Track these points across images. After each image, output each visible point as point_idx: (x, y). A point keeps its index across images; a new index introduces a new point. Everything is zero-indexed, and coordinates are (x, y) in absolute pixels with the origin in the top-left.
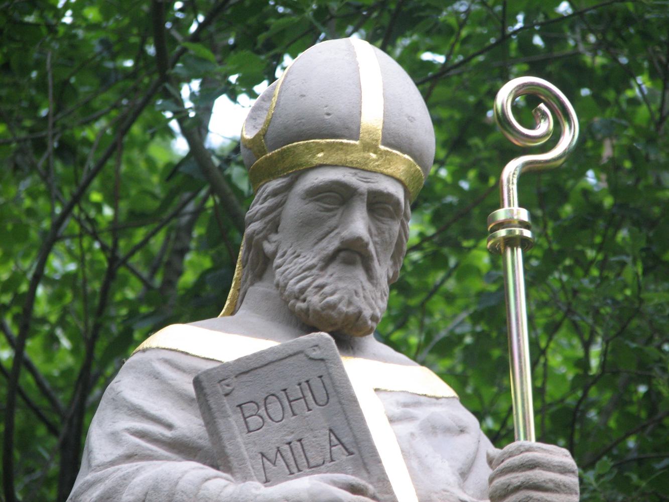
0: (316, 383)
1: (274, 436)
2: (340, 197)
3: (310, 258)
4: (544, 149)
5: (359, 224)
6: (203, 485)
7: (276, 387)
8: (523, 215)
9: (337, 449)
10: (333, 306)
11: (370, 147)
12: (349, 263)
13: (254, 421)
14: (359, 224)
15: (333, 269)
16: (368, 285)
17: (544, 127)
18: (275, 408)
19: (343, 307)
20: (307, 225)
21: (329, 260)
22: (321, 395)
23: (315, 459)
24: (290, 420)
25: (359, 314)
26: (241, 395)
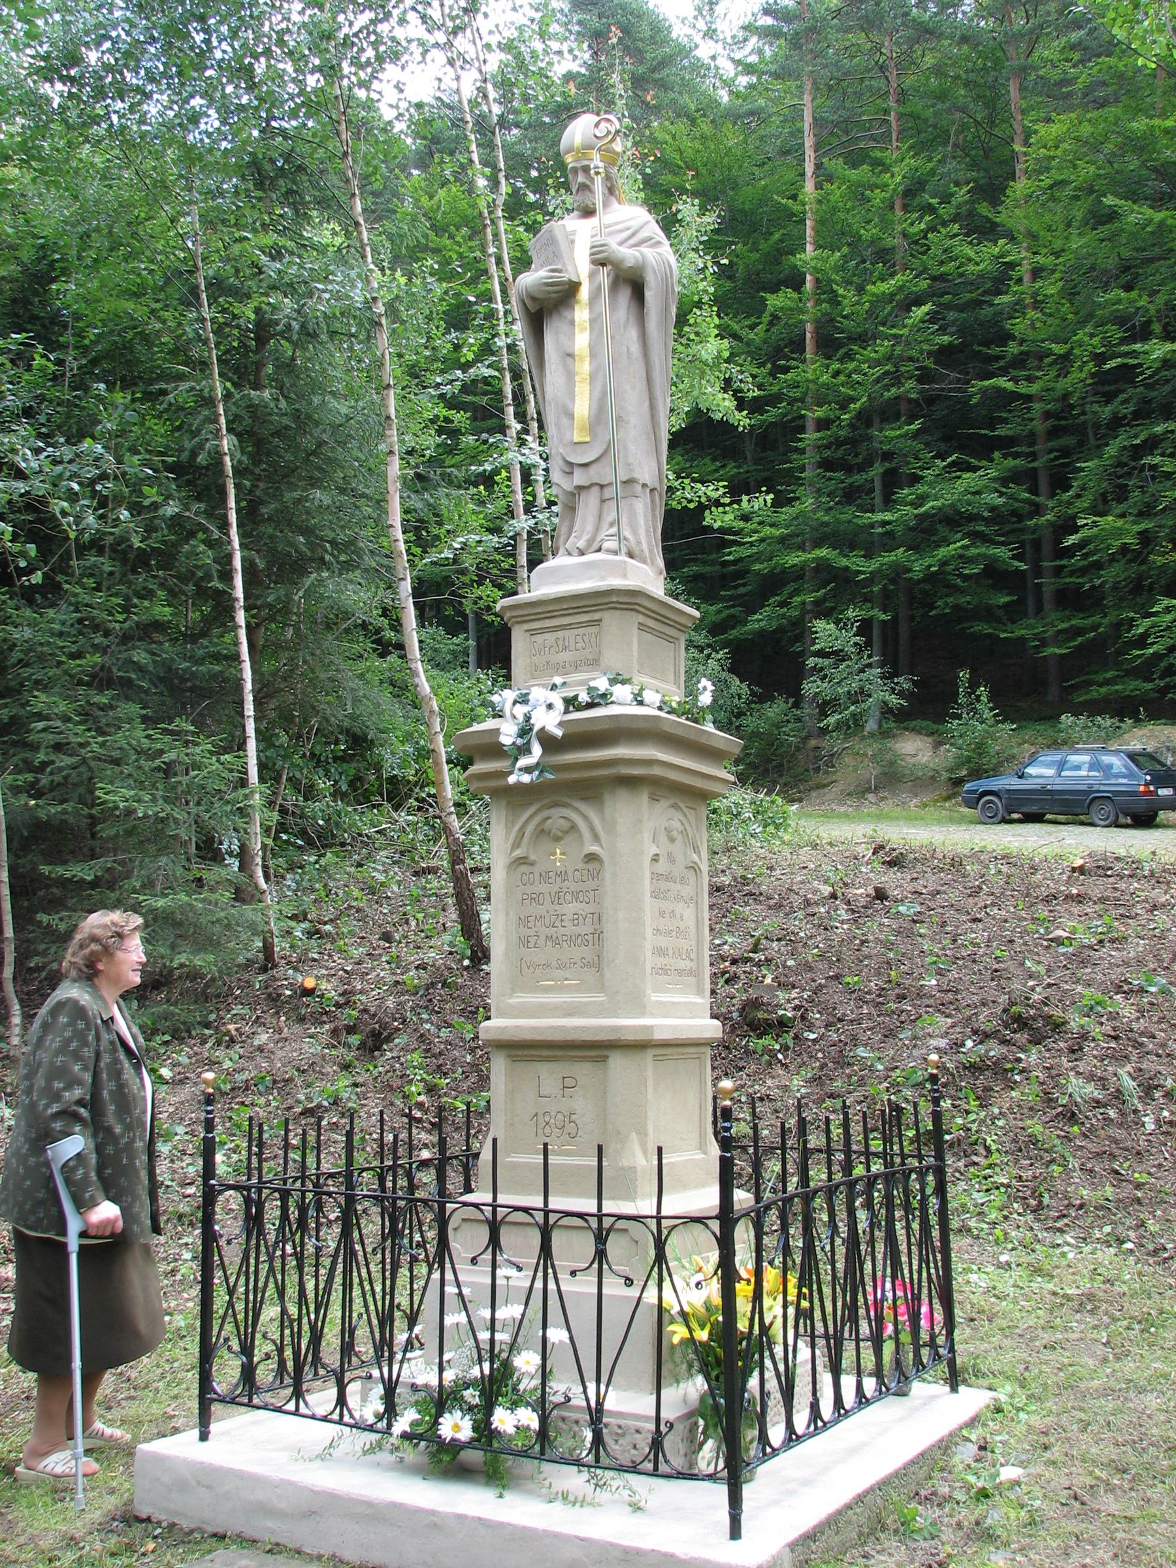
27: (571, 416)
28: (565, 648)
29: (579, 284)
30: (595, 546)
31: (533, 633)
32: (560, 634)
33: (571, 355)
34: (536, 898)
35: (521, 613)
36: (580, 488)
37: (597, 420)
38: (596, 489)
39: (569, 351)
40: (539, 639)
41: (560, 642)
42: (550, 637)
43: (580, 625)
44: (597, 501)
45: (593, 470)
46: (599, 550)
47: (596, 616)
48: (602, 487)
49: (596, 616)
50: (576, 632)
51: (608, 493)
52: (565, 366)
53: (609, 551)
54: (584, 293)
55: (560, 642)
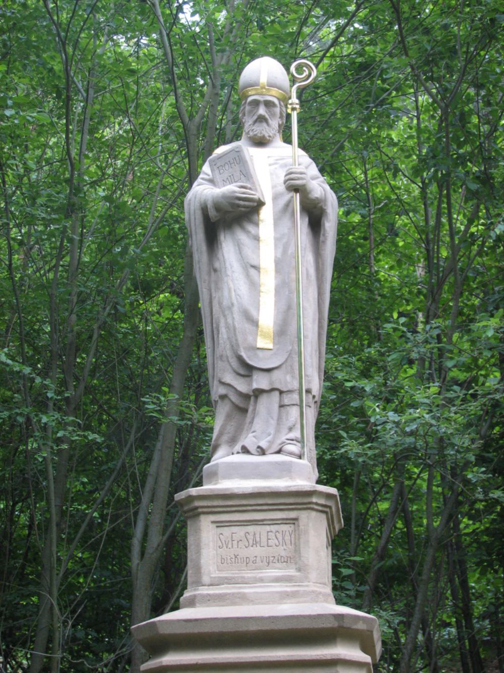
0: (237, 158)
1: (226, 175)
2: (256, 103)
3: (251, 122)
4: (307, 79)
5: (262, 111)
6: (190, 195)
7: (227, 161)
8: (297, 101)
9: (242, 176)
10: (256, 135)
11: (263, 88)
12: (261, 122)
13: (222, 171)
14: (262, 111)
15: (257, 124)
16: (267, 127)
17: (306, 73)
18: (227, 167)
19: (259, 135)
20: (250, 112)
21: (255, 122)
22: (238, 161)
23: (236, 180)
24: (231, 170)
25: (264, 136)
26: (218, 165)
27: (255, 323)
28: (255, 543)
29: (261, 204)
30: (276, 448)
31: (219, 524)
32: (251, 529)
33: (256, 268)
34: (125, 582)
35: (215, 503)
36: (258, 393)
37: (281, 332)
38: (277, 393)
39: (254, 263)
40: (227, 531)
41: (250, 537)
42: (240, 531)
43: (274, 522)
44: (276, 406)
45: (276, 374)
46: (279, 452)
47: (293, 515)
48: (281, 392)
49: (293, 515)
50: (268, 528)
51: (287, 400)
52: (248, 276)
53: (291, 454)
54: (266, 214)
55: (250, 537)
